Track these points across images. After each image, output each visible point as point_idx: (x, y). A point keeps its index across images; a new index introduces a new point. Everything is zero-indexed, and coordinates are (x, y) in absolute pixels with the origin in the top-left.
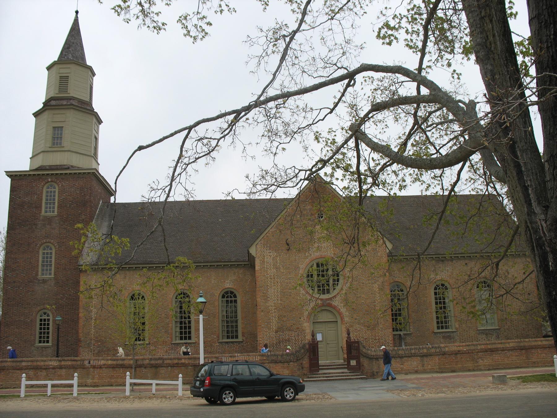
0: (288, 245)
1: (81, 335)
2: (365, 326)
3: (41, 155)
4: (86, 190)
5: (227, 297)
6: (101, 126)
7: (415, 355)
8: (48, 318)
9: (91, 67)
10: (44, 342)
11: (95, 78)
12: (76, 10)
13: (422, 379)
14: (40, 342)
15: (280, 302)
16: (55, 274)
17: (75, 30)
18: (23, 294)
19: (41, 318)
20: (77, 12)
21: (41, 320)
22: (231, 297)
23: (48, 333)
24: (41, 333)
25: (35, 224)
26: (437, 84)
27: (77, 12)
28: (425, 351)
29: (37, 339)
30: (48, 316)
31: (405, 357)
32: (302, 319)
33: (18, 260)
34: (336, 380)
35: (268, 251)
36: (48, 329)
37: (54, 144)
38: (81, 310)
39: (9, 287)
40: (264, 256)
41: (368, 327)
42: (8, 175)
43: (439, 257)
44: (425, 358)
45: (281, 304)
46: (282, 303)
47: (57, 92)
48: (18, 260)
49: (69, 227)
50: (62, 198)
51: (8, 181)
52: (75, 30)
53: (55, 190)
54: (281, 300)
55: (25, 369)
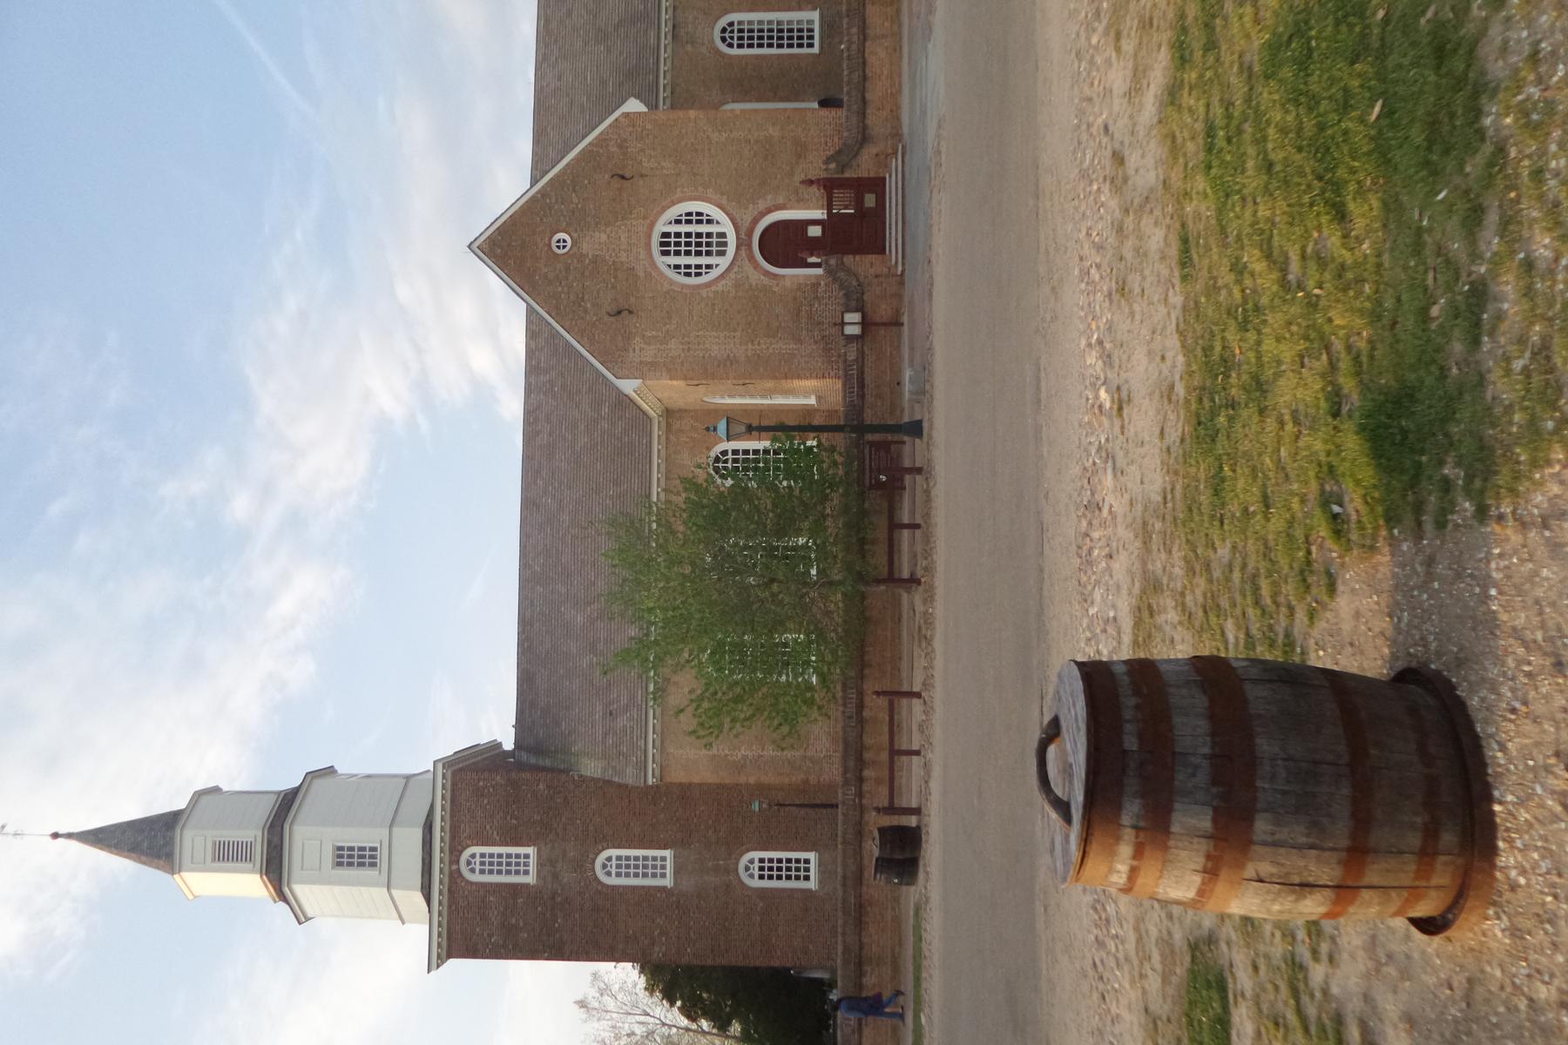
0: (619, 313)
1: (794, 779)
2: (797, 163)
3: (393, 892)
4: (481, 783)
5: (732, 38)
6: (341, 769)
7: (862, 51)
8: (756, 861)
9: (195, 793)
10: (807, 870)
11: (225, 788)
12: (49, 838)
13: (870, 468)
14: (807, 878)
15: (738, 334)
16: (665, 848)
17: (101, 838)
18: (704, 918)
19: (756, 876)
20: (55, 836)
21: (762, 877)
22: (732, 32)
23: (789, 861)
24: (789, 878)
25: (553, 898)
26: (486, 960)
27: (55, 836)
28: (854, 30)
29: (801, 885)
30: (752, 861)
31: (864, 71)
32: (776, 289)
33: (631, 932)
34: (903, 197)
35: (631, 354)
36: (780, 861)
37: (373, 865)
38: (742, 780)
39: (689, 950)
40: (641, 362)
41: (799, 156)
42: (438, 966)
43: (665, 72)
44: (870, 32)
45: (743, 330)
46: (740, 329)
47: (251, 865)
48: (631, 932)
49: (563, 819)
50: (498, 838)
51: (454, 964)
52: (101, 838)
53: (478, 856)
54: (735, 330)
55: (862, 858)
